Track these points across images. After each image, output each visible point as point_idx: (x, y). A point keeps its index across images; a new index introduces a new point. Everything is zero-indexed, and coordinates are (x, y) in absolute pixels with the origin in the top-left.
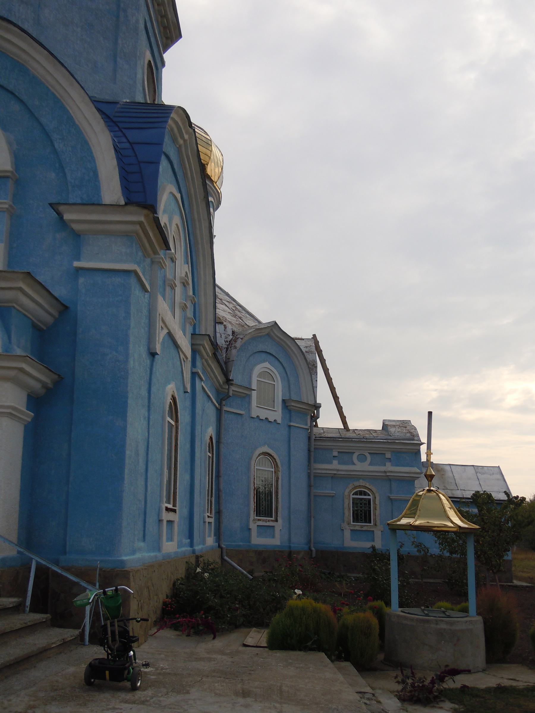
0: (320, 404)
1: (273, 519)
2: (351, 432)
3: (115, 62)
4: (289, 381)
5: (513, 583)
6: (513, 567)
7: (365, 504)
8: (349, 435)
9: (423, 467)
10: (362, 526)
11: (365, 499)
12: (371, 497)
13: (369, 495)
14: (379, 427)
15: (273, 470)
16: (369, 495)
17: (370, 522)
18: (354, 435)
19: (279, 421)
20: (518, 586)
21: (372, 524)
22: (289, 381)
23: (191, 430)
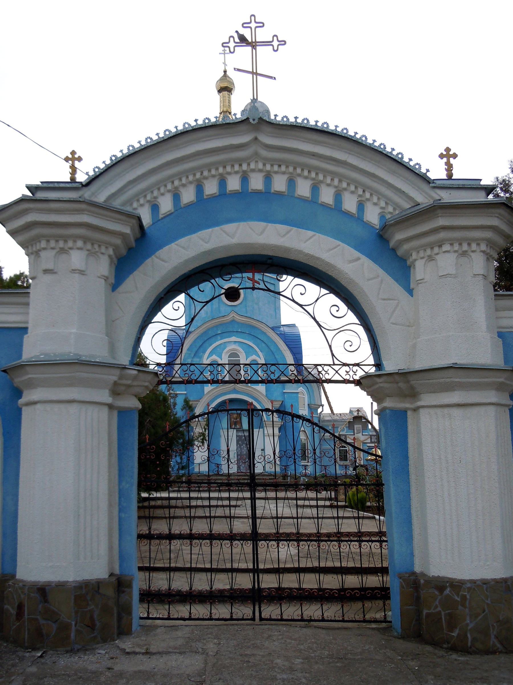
0: (323, 405)
1: (307, 461)
2: (336, 415)
3: (276, 312)
4: (310, 394)
5: (492, 194)
6: (245, 453)
7: (345, 452)
8: (336, 418)
9: (370, 431)
10: (344, 463)
11: (344, 450)
12: (347, 449)
13: (346, 448)
14: (348, 412)
15: (306, 438)
16: (346, 448)
17: (347, 461)
18: (338, 418)
19: (307, 415)
20: (386, 186)
21: (348, 462)
22: (310, 394)
23: (409, 478)
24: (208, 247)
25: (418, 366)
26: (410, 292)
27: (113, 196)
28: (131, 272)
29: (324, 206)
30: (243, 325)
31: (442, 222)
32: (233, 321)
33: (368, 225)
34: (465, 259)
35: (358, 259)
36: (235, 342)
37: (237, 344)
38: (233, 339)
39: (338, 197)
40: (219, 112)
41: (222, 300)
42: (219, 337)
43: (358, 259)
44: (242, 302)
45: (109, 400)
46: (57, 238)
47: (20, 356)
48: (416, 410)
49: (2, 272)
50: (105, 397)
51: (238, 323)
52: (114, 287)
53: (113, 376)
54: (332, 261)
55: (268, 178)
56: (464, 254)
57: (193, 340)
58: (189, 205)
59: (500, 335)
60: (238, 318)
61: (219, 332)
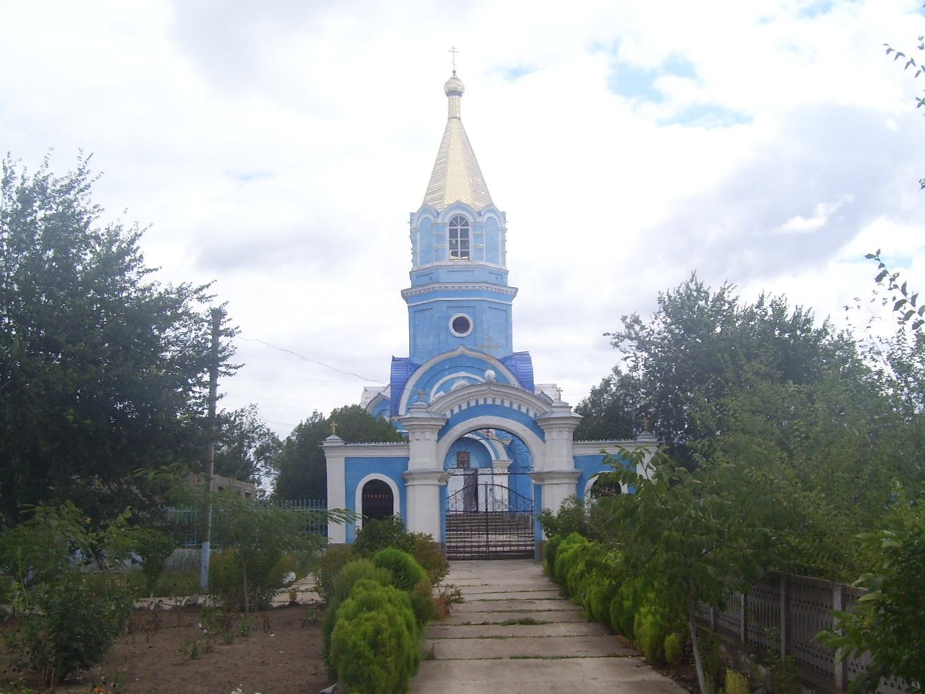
24: (471, 425)
25: (545, 470)
26: (544, 442)
27: (437, 410)
28: (443, 435)
29: (514, 410)
30: (472, 359)
31: (552, 422)
32: (462, 356)
33: (530, 417)
34: (560, 434)
35: (526, 430)
36: (464, 378)
37: (466, 379)
38: (462, 374)
39: (519, 407)
40: (447, 117)
41: (450, 331)
42: (447, 373)
43: (526, 430)
44: (471, 333)
45: (438, 483)
46: (421, 428)
47: (407, 469)
48: (544, 484)
49: (350, 406)
50: (436, 482)
51: (467, 357)
52: (437, 441)
53: (439, 475)
54: (516, 431)
55: (494, 400)
56: (560, 432)
57: (420, 375)
58: (464, 410)
59: (574, 458)
60: (467, 352)
61: (447, 367)
